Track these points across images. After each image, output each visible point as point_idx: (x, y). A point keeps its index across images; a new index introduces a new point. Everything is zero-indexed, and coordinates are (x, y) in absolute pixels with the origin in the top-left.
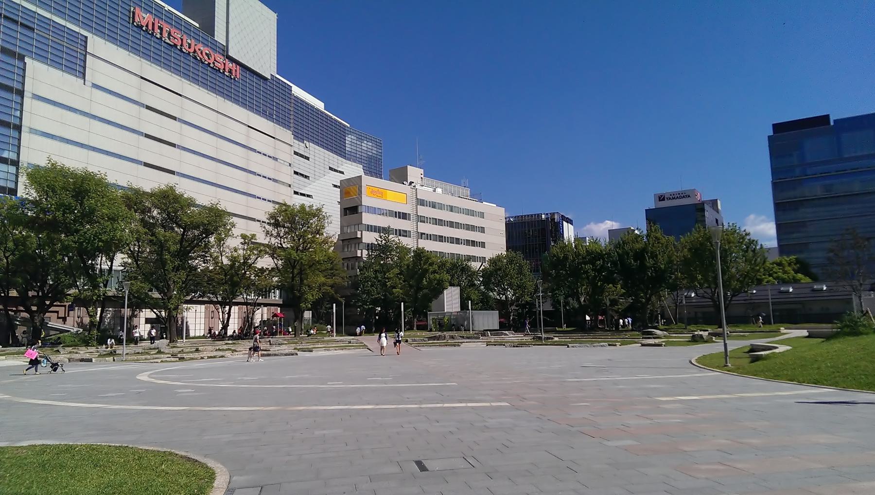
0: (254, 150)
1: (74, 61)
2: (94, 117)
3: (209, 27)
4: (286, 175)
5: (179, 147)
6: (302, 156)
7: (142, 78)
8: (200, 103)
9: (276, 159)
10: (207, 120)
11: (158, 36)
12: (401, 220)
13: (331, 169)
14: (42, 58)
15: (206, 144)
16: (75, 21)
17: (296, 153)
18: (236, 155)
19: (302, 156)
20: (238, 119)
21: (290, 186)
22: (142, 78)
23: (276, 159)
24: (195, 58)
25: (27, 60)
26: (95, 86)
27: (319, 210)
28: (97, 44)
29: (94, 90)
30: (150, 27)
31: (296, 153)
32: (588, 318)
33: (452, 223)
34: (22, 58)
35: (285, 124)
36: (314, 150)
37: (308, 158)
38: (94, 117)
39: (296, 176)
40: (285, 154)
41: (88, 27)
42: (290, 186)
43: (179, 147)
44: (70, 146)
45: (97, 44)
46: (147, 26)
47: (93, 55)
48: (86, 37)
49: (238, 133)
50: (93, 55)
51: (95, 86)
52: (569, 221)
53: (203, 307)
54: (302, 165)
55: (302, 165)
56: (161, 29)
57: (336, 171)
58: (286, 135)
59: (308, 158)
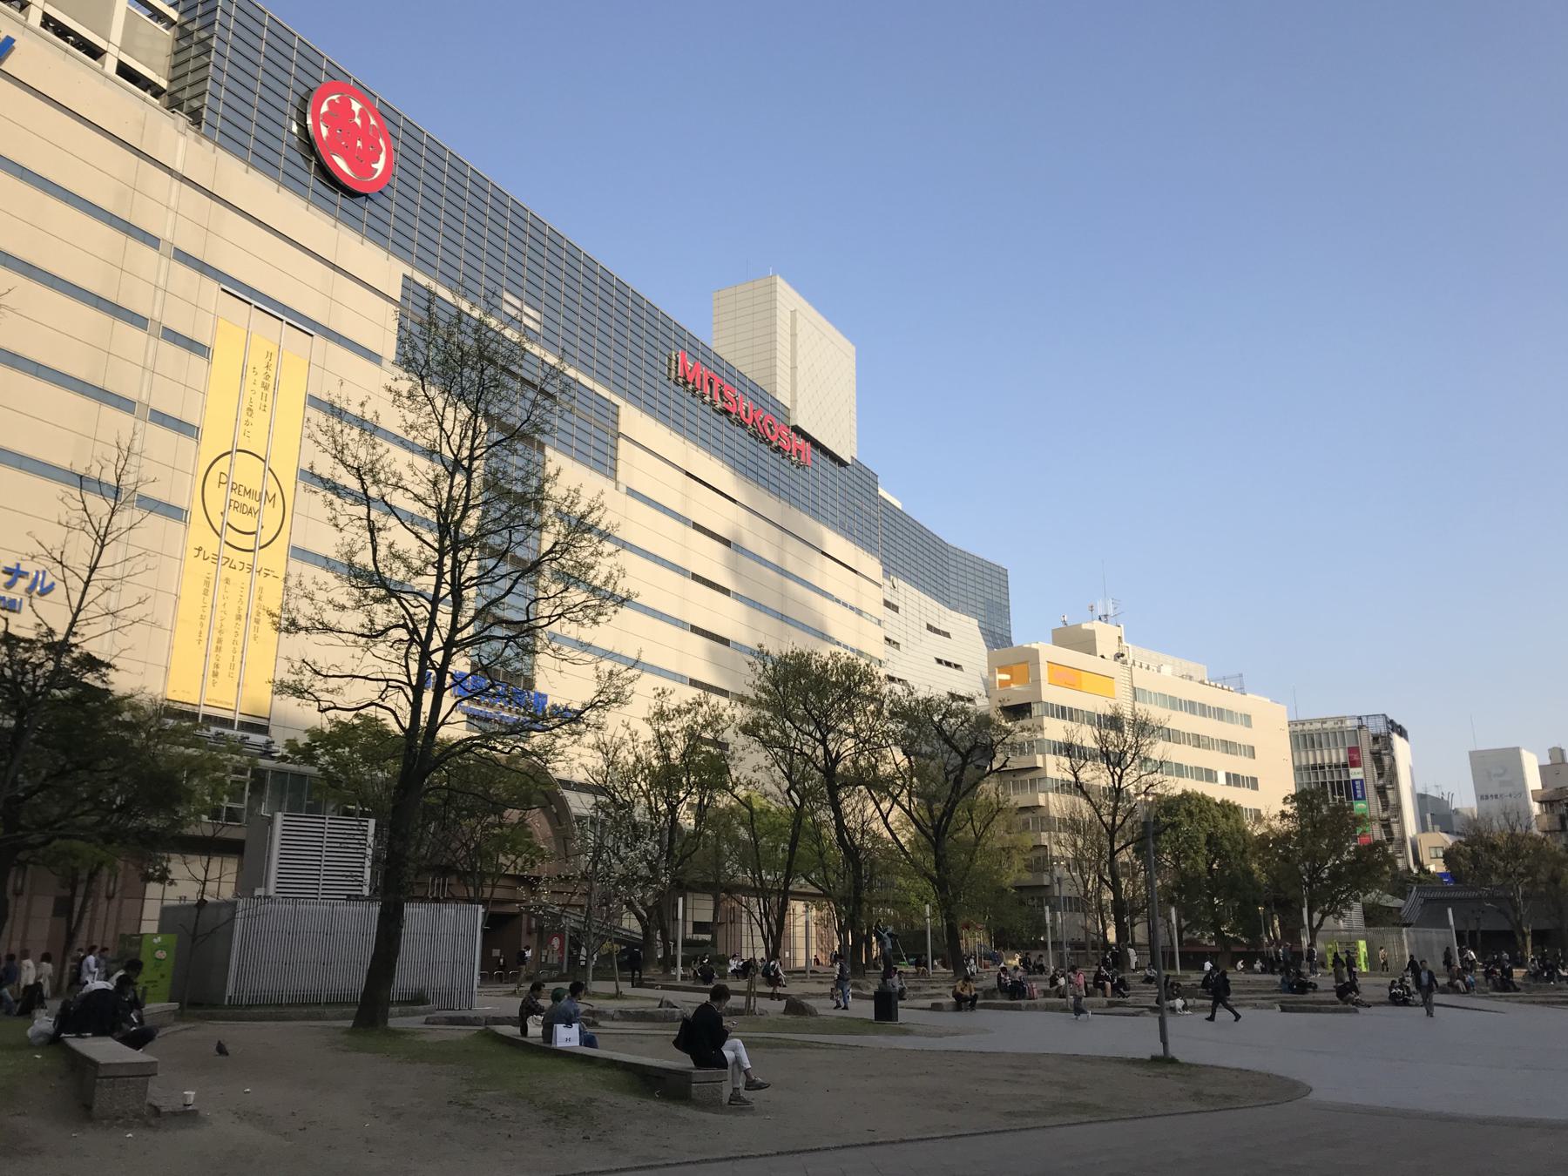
5: (682, 571)
7: (688, 474)
9: (860, 612)
12: (1205, 766)
13: (930, 628)
16: (601, 377)
22: (688, 474)
23: (860, 612)
26: (631, 492)
28: (633, 420)
29: (629, 499)
32: (359, 144)
33: (1192, 704)
36: (907, 594)
40: (871, 599)
41: (618, 388)
43: (682, 571)
45: (633, 420)
47: (628, 439)
50: (628, 439)
51: (631, 492)
52: (1402, 733)
53: (411, 910)
57: (937, 631)
58: (871, 565)
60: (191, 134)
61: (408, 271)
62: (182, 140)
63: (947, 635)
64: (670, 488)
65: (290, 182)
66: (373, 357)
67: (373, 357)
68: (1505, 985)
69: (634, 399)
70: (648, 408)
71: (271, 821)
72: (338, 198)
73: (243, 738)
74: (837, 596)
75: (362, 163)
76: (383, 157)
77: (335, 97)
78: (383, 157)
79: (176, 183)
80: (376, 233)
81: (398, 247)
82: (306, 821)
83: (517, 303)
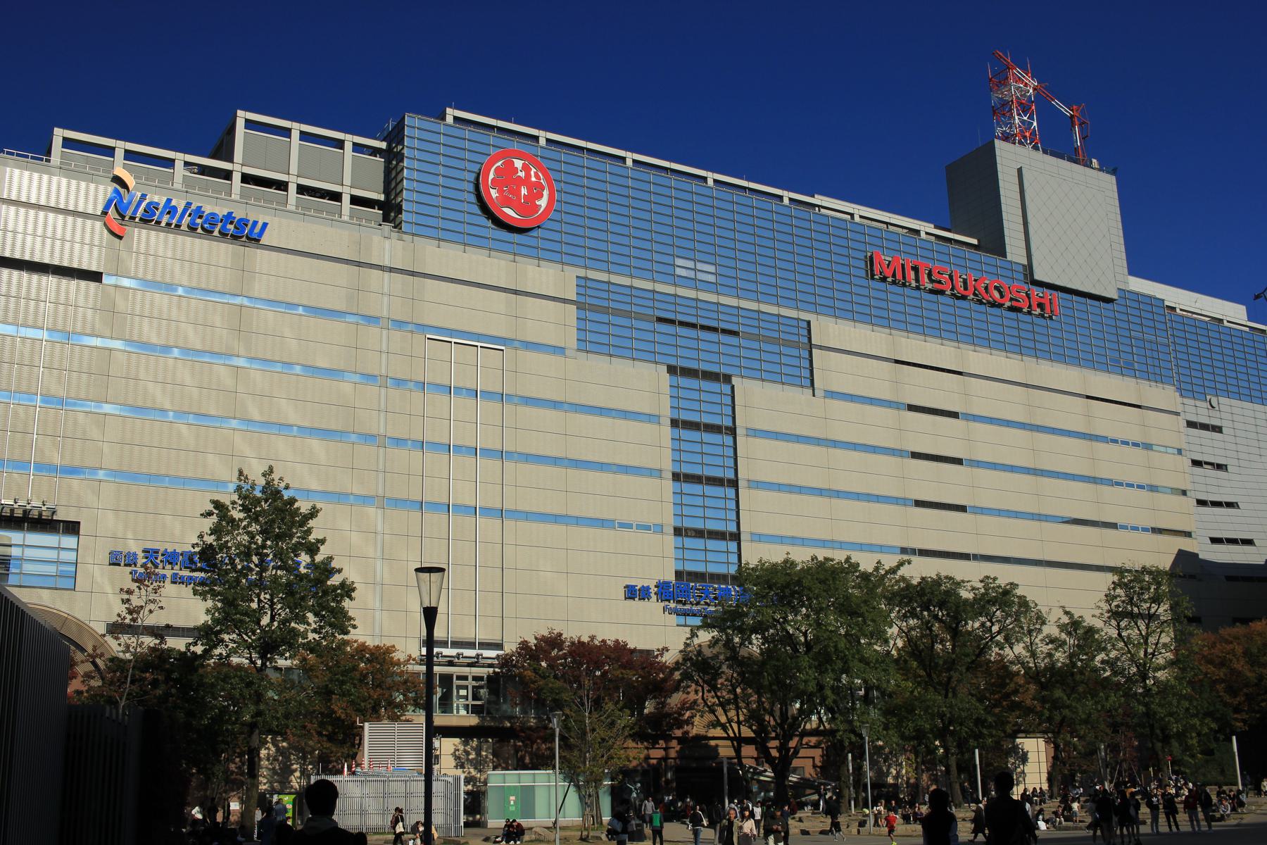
0: (1105, 439)
1: (796, 360)
2: (835, 444)
3: (994, 243)
4: (1175, 471)
6: (1205, 427)
8: (991, 377)
9: (1148, 447)
10: (1010, 404)
11: (914, 284)
14: (761, 375)
15: (1013, 448)
17: (1191, 424)
18: (1069, 456)
19: (1205, 427)
20: (1064, 386)
21: (1184, 493)
23: (1148, 447)
24: (980, 302)
25: (735, 381)
26: (831, 394)
27: (347, 590)
28: (827, 329)
30: (899, 276)
31: (1191, 424)
34: (727, 379)
35: (1154, 374)
37: (1218, 429)
38: (835, 444)
39: (1197, 470)
40: (1169, 431)
42: (1184, 493)
44: (846, 502)
45: (827, 329)
46: (894, 275)
47: (565, 301)
48: (809, 323)
49: (1069, 413)
50: (565, 301)
54: (1208, 447)
55: (1208, 447)
56: (915, 269)
58: (1162, 395)
59: (1218, 429)
60: (395, 235)
61: (582, 272)
62: (387, 242)
63: (1020, 171)
64: (879, 380)
65: (467, 240)
66: (559, 350)
67: (559, 350)
68: (931, 598)
69: (816, 308)
70: (837, 312)
71: (362, 728)
72: (516, 237)
73: (478, 655)
74: (1111, 435)
75: (529, 206)
76: (546, 193)
77: (499, 164)
78: (546, 193)
79: (387, 275)
80: (540, 255)
81: (558, 254)
82: (376, 725)
83: (690, 264)
